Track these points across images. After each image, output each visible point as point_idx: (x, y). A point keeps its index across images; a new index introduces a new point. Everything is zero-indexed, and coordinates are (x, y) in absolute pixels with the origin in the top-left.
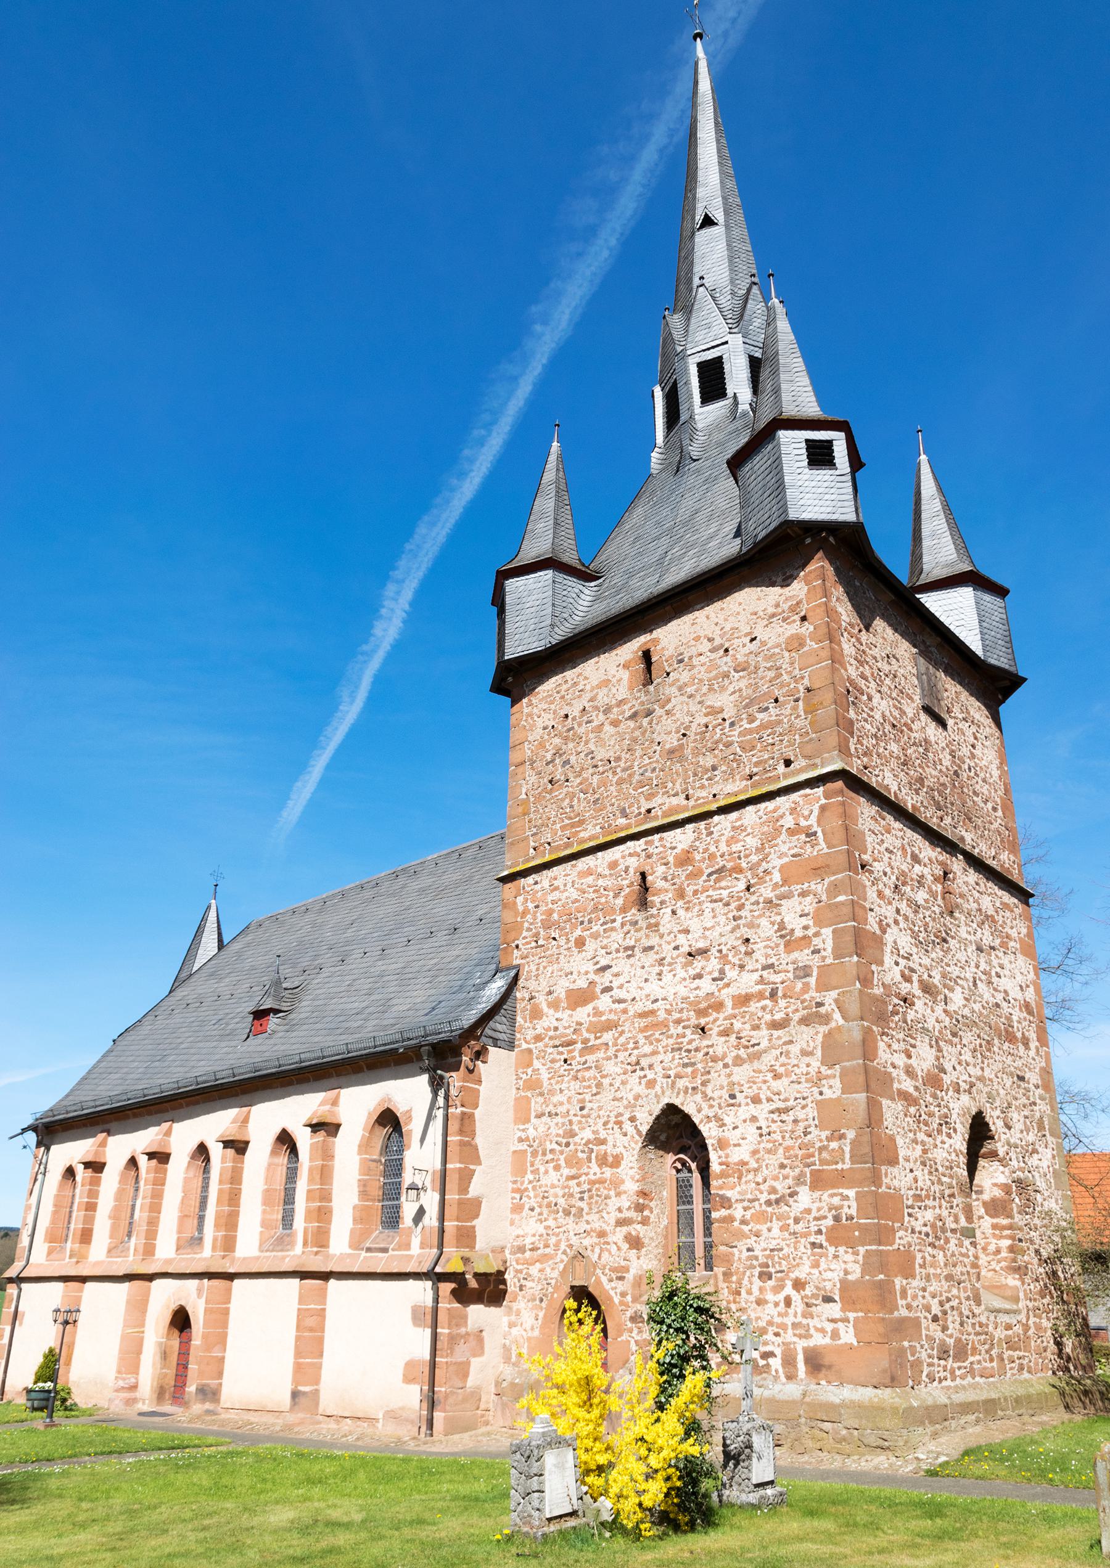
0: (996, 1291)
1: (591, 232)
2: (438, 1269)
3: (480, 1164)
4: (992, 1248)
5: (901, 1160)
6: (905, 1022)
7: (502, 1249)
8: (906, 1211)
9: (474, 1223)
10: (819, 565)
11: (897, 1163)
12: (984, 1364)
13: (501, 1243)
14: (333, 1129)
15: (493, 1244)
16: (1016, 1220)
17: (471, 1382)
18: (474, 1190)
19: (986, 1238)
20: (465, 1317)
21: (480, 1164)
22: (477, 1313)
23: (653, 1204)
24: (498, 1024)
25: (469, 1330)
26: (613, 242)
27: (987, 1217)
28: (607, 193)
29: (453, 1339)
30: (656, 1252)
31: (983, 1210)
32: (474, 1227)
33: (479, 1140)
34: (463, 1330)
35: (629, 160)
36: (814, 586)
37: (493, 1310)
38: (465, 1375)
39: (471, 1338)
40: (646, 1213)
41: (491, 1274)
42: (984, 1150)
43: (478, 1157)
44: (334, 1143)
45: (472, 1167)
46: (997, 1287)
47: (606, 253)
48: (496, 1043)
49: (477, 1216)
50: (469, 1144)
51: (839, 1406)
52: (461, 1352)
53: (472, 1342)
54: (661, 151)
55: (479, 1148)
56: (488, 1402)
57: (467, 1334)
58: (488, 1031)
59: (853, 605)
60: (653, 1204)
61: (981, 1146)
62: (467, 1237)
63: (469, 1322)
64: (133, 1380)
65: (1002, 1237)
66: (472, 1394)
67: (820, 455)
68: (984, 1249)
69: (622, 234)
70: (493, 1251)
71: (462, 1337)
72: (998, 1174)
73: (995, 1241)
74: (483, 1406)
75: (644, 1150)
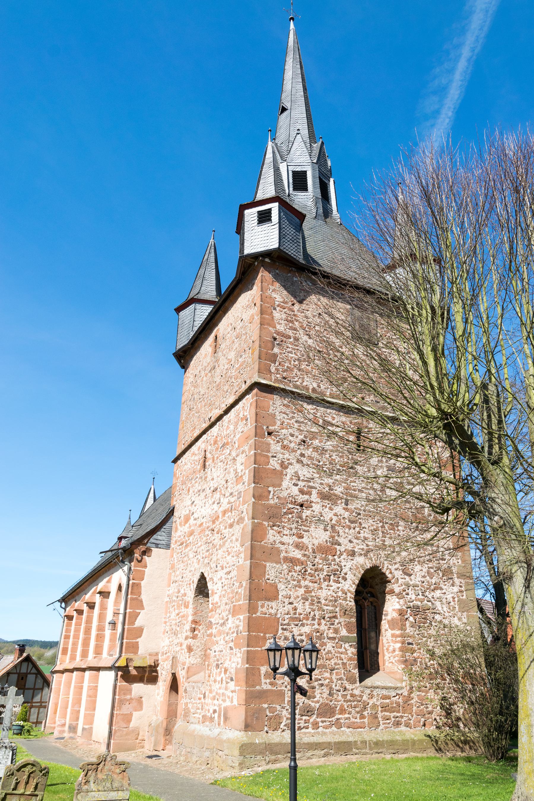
0: (392, 675)
1: (437, 113)
2: (116, 665)
3: (143, 609)
4: (391, 649)
5: (280, 597)
6: (301, 518)
7: (157, 654)
8: (280, 627)
9: (137, 640)
10: (263, 275)
11: (278, 599)
12: (353, 720)
13: (156, 651)
14: (107, 594)
15: (150, 651)
16: (408, 631)
17: (132, 725)
18: (138, 623)
19: (388, 643)
20: (130, 690)
21: (143, 609)
22: (138, 688)
23: (200, 628)
24: (160, 536)
25: (132, 696)
26: (450, 114)
27: (389, 630)
28: (442, 91)
29: (121, 702)
30: (200, 654)
31: (387, 626)
32: (138, 642)
33: (143, 597)
34: (128, 697)
35: (451, 71)
36: (266, 287)
37: (153, 686)
38: (129, 721)
39: (134, 701)
40: (196, 632)
41: (146, 667)
42: (387, 589)
43: (143, 606)
44: (107, 602)
45: (137, 611)
46: (393, 673)
47: (447, 121)
48: (157, 546)
49: (140, 636)
50: (136, 599)
51: (225, 741)
52: (126, 709)
53: (134, 704)
54: (469, 60)
55: (144, 601)
56: (143, 736)
57: (131, 699)
58: (152, 540)
59: (288, 292)
60: (200, 628)
61: (386, 587)
62: (134, 648)
63: (133, 693)
64: (63, 721)
65: (396, 642)
66: (133, 731)
67: (264, 218)
68: (387, 649)
69: (454, 109)
70: (150, 655)
71: (127, 700)
72: (396, 603)
73: (392, 644)
74: (140, 738)
75: (196, 598)
